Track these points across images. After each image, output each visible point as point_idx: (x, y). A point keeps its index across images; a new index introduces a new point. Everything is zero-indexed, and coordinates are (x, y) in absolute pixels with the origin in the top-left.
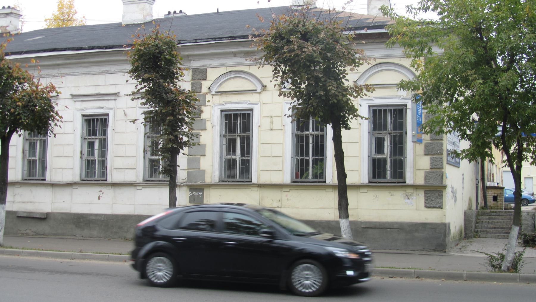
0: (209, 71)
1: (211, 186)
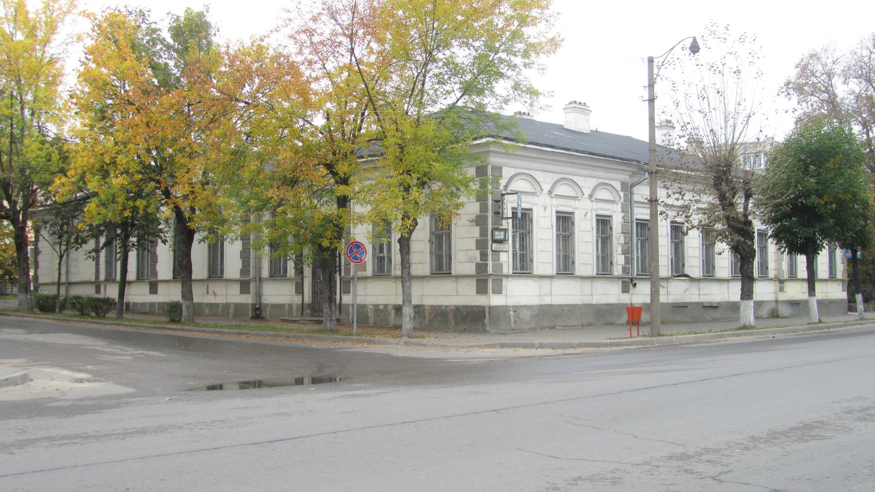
0: (504, 169)
1: (507, 276)
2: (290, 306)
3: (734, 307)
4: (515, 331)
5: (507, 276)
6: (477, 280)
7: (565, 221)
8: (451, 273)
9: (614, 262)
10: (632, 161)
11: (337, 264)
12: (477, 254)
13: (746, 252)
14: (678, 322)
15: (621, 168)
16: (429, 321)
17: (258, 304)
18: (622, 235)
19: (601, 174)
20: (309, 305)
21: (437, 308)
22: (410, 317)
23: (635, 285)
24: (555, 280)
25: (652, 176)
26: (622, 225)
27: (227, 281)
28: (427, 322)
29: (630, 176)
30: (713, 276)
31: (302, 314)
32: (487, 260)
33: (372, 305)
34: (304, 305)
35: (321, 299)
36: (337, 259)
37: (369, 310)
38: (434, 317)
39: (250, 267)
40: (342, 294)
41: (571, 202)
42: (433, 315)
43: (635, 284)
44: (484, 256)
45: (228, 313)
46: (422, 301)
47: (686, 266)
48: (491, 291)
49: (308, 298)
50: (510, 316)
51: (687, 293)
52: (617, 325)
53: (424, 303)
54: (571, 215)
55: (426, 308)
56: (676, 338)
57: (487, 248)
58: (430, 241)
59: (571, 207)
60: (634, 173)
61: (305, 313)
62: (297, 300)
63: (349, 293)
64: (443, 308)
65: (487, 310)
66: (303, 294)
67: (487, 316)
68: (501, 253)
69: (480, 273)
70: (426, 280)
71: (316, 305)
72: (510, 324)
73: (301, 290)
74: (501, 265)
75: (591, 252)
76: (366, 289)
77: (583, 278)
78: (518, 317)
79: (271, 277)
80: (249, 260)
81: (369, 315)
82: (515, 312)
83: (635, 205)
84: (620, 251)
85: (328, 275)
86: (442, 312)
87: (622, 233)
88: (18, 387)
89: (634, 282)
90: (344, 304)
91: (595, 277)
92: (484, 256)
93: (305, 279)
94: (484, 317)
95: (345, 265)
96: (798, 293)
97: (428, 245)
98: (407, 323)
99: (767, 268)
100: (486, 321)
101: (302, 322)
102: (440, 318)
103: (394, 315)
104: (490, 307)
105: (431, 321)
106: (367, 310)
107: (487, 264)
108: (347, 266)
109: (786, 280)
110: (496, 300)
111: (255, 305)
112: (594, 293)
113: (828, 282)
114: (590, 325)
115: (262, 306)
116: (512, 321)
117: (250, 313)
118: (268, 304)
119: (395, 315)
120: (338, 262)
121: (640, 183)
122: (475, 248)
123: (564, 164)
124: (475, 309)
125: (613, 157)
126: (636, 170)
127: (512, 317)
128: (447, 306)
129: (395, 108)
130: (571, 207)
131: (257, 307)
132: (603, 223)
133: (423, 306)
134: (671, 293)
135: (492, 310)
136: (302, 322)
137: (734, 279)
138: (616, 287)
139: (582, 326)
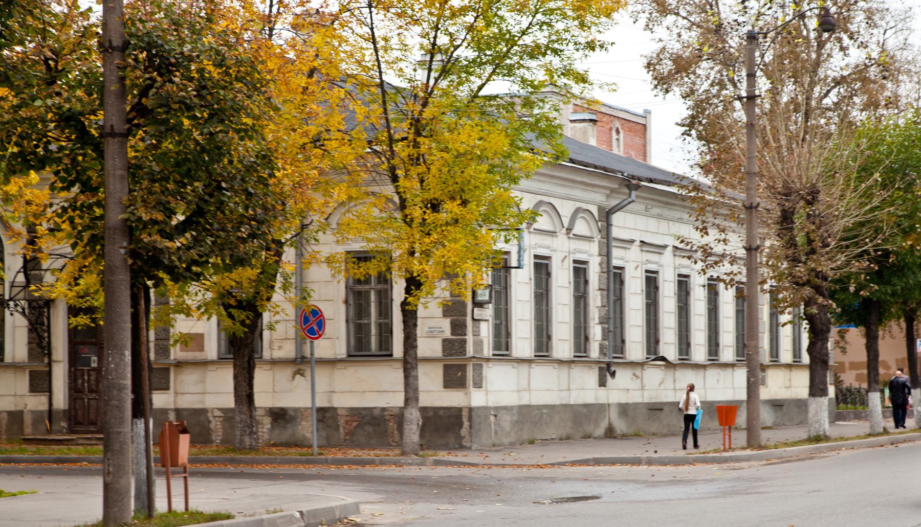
1: (488, 360)
3: (801, 405)
4: (496, 447)
5: (488, 360)
6: (445, 366)
7: (652, 282)
8: (391, 355)
9: (591, 336)
10: (613, 171)
12: (446, 324)
13: (822, 324)
14: (654, 434)
15: (602, 184)
16: (347, 434)
18: (599, 292)
19: (577, 193)
21: (364, 413)
22: (418, 424)
23: (613, 374)
24: (533, 365)
25: (751, 212)
26: (599, 276)
28: (342, 436)
29: (608, 196)
30: (800, 362)
32: (465, 335)
33: (219, 409)
37: (211, 419)
38: (356, 427)
41: (547, 240)
42: (355, 424)
43: (614, 372)
44: (458, 327)
46: (330, 401)
47: (661, 343)
48: (471, 383)
49: (60, 399)
50: (491, 422)
51: (663, 387)
52: (595, 438)
53: (336, 405)
54: (506, 257)
55: (339, 412)
56: (785, 451)
57: (466, 316)
58: (346, 302)
59: (548, 248)
60: (612, 191)
62: (38, 403)
63: (167, 388)
64: (377, 412)
65: (465, 414)
66: (50, 391)
67: (466, 424)
69: (451, 355)
70: (339, 366)
71: (80, 412)
72: (491, 436)
73: (46, 386)
74: (482, 341)
75: (568, 321)
76: (203, 381)
77: (561, 362)
78: (499, 425)
81: (212, 426)
82: (495, 416)
83: (614, 244)
84: (597, 321)
85: (246, 359)
86: (374, 418)
87: (600, 289)
88: (641, 467)
89: (613, 369)
91: (573, 362)
92: (458, 327)
94: (461, 425)
95: (156, 339)
96: (780, 388)
97: (343, 307)
98: (412, 434)
100: (464, 431)
101: (81, 441)
102: (369, 429)
103: (269, 426)
104: (471, 409)
105: (350, 433)
106: (207, 418)
107: (465, 341)
108: (161, 342)
109: (768, 366)
110: (477, 399)
112: (571, 388)
113: (573, 366)
114: (568, 438)
116: (493, 431)
119: (273, 427)
121: (621, 208)
122: (441, 315)
123: (542, 178)
124: (441, 412)
125: (596, 167)
126: (616, 186)
127: (492, 425)
128: (384, 409)
130: (548, 248)
132: (580, 271)
133: (335, 409)
134: (646, 388)
135: (473, 414)
136: (81, 441)
137: (221, 359)
138: (591, 377)
139: (561, 439)
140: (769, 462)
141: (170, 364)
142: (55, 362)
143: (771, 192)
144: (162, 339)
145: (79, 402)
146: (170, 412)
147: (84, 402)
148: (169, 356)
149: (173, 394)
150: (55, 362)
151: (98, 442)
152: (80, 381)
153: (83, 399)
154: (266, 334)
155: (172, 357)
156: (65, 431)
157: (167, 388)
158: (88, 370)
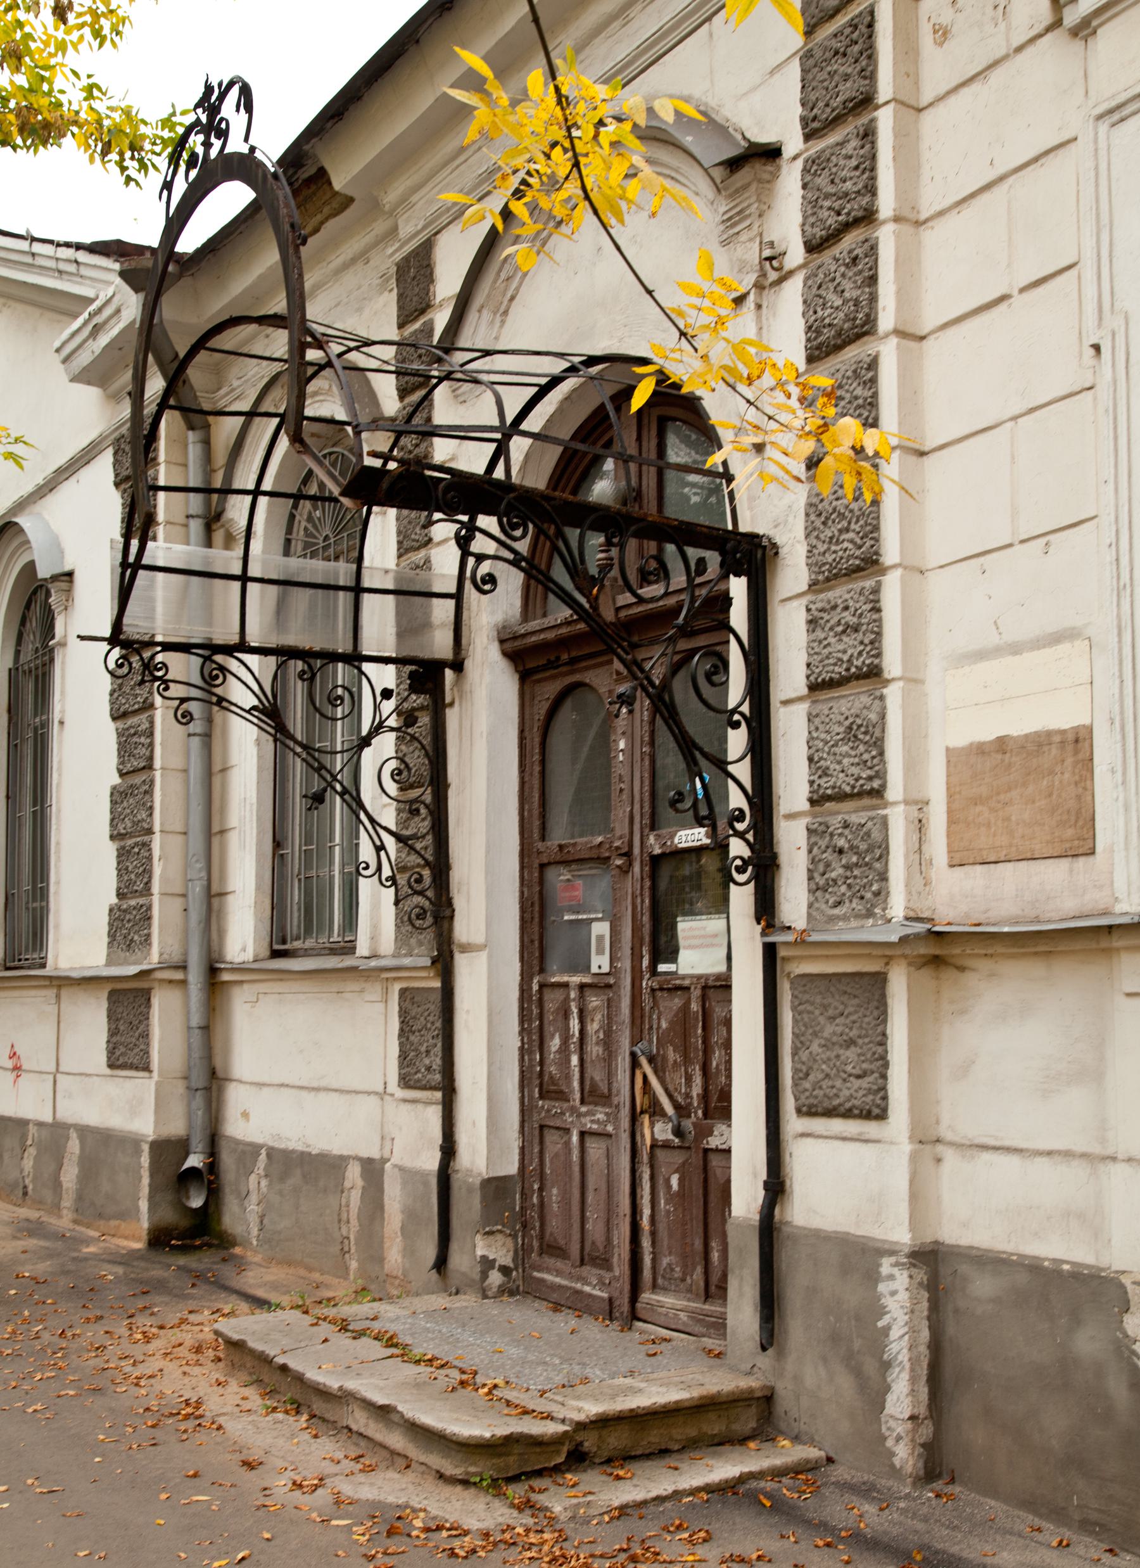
2: (373, 1170)
11: (737, 800)
17: (198, 1144)
20: (495, 1188)
27: (62, 983)
31: (441, 1263)
34: (457, 1181)
35: (593, 1145)
36: (737, 741)
39: (147, 890)
40: (792, 1123)
45: (57, 1185)
61: (459, 1261)
63: (876, 1112)
68: (382, 1005)
79: (276, 954)
80: (147, 846)
90: (819, 1237)
93: (462, 962)
99: (632, 949)
101: (359, 1420)
108: (838, 814)
111: (182, 1147)
115: (228, 1161)
117: (144, 1205)
118: (255, 1149)
120: (742, 771)
129: (830, 522)
131: (194, 1161)
140: (509, 542)
141: (886, 951)
142: (466, 948)
143: (854, 1106)
144: (842, 797)
145: (553, 1142)
146: (886, 1266)
147: (568, 1144)
148: (882, 895)
149: (907, 1148)
150: (466, 948)
151: (413, 1452)
152: (555, 1043)
153: (567, 1131)
154: (552, 697)
155: (897, 907)
156: (495, 1278)
157: (876, 1112)
158: (582, 987)
